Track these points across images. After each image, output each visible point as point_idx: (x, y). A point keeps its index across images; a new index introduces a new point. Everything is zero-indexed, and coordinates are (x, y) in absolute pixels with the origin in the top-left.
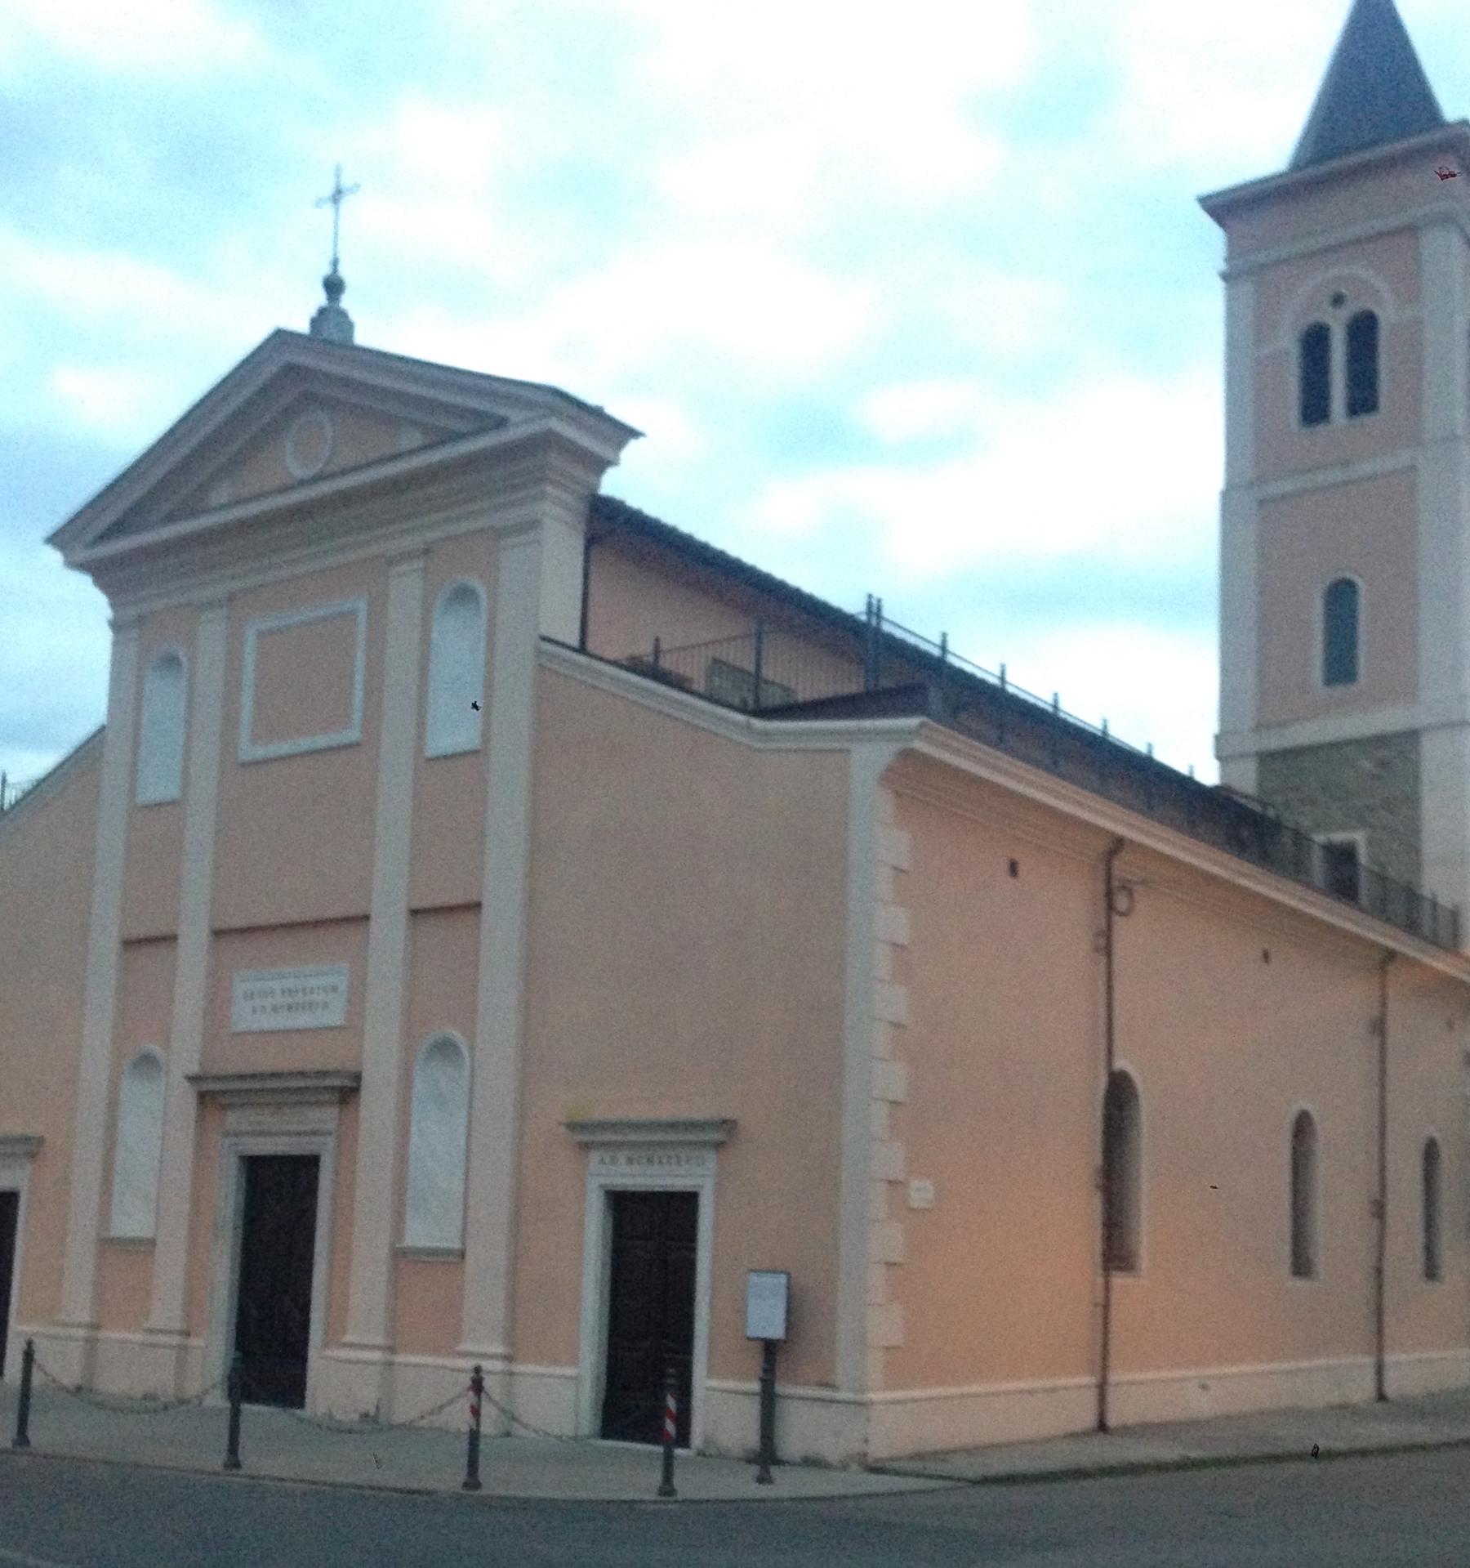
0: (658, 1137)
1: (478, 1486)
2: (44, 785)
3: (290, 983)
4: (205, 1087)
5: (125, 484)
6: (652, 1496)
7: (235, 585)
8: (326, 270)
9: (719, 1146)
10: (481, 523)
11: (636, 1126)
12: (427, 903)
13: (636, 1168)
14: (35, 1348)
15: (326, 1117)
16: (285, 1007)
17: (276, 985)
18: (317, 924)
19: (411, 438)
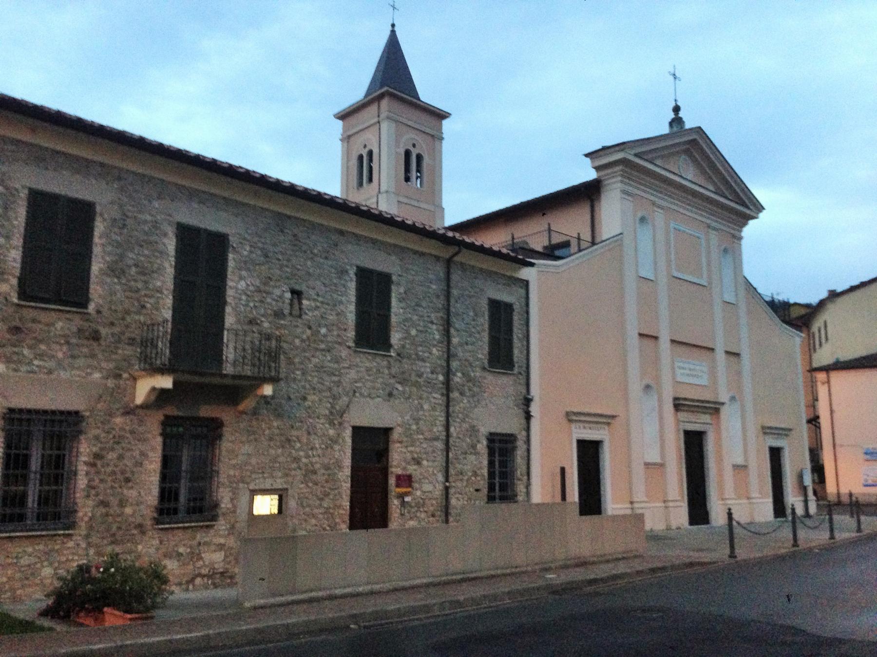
0: (595, 419)
1: (735, 557)
2: (797, 307)
3: (692, 367)
4: (677, 402)
5: (633, 144)
6: (726, 557)
7: (714, 224)
8: (673, 104)
9: (609, 424)
10: (652, 198)
11: (589, 415)
12: (645, 332)
13: (585, 431)
14: (733, 511)
15: (706, 418)
16: (693, 376)
17: (686, 366)
18: (694, 346)
19: (711, 188)
